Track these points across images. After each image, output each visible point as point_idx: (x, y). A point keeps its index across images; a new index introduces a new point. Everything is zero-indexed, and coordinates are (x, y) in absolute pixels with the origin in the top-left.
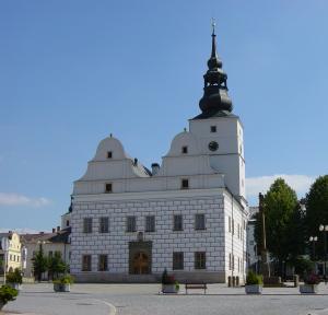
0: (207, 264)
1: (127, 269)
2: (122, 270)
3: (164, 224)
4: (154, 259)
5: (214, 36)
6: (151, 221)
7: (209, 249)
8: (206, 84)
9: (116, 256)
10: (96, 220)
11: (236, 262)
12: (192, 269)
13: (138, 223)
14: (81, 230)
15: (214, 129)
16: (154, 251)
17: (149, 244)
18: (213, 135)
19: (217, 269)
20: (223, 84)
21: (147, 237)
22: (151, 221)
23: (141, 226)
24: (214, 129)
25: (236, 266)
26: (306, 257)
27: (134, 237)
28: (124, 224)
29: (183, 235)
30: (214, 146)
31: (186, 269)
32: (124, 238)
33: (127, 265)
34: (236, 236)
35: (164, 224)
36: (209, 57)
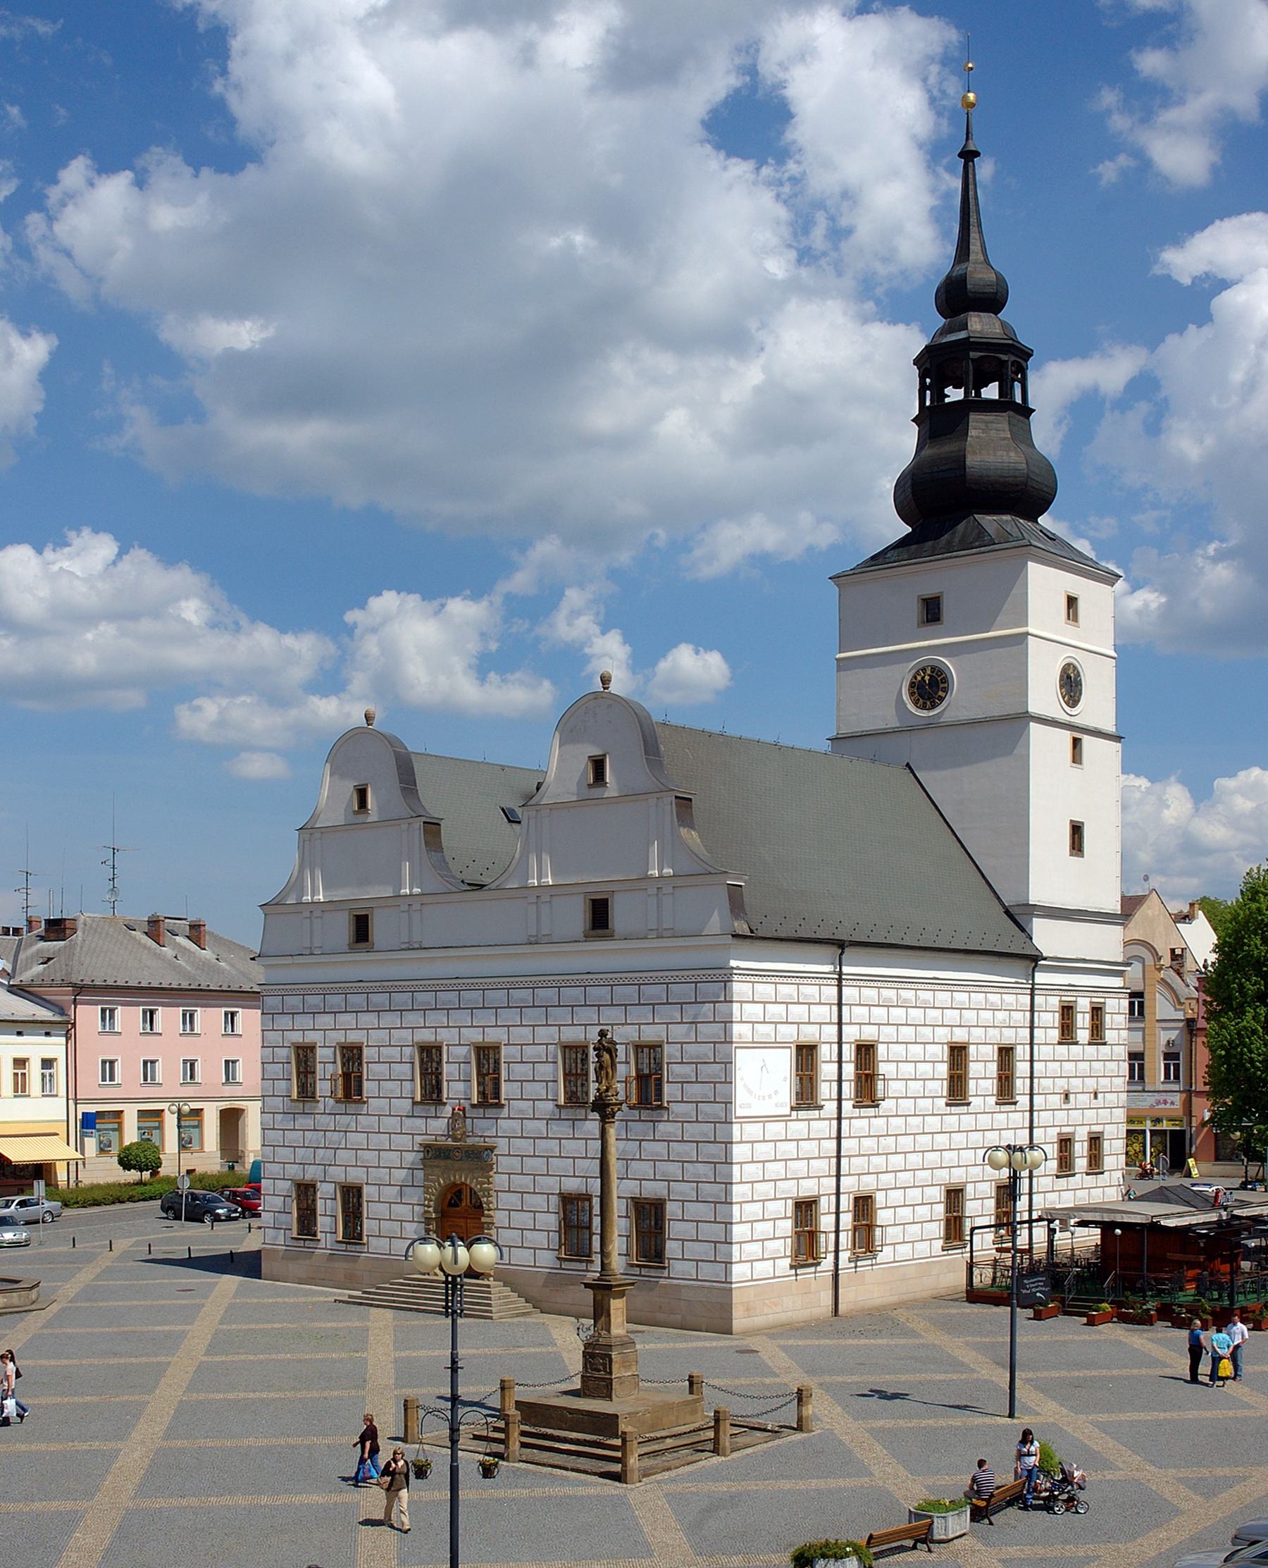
16: (499, 1181)
17: (480, 1157)
23: (459, 1085)
35: (533, 1080)
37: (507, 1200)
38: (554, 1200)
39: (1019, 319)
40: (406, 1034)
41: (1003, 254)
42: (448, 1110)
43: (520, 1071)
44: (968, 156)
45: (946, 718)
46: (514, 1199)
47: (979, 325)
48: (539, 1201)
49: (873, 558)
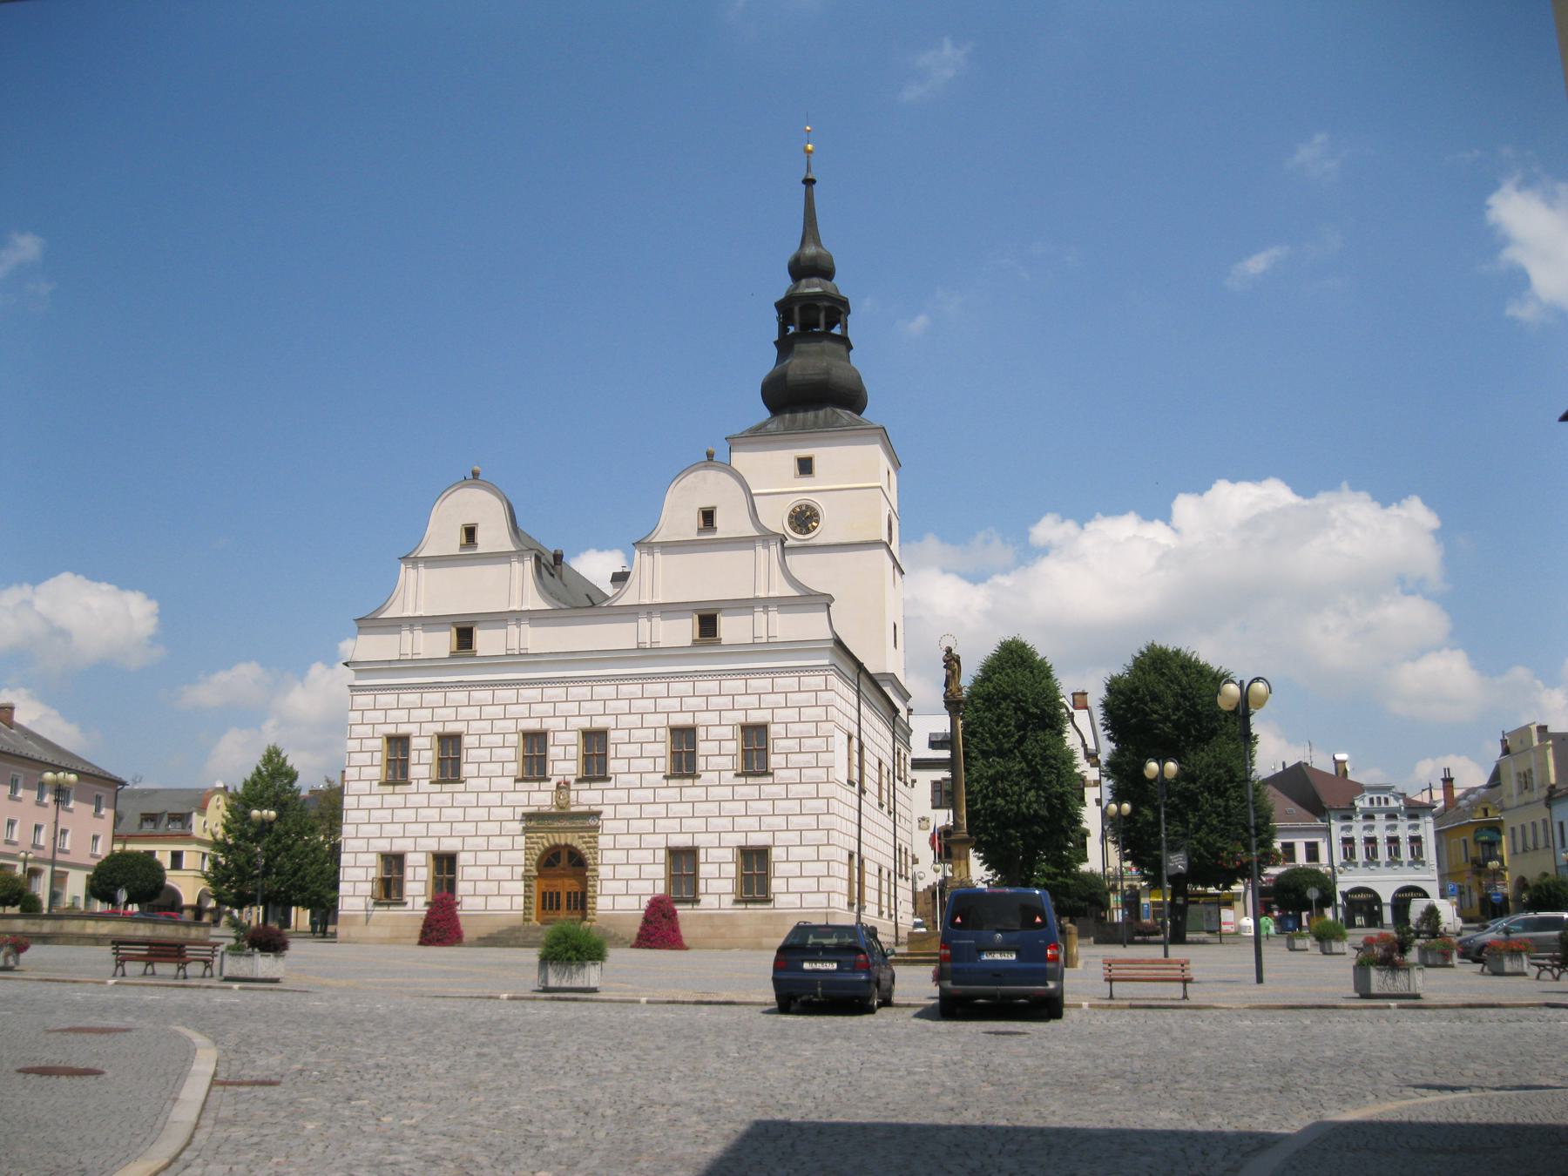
0: (776, 885)
1: (519, 902)
2: (504, 903)
3: (639, 755)
4: (604, 871)
5: (809, 182)
6: (595, 743)
7: (782, 837)
8: (783, 328)
9: (485, 857)
10: (426, 742)
11: (871, 881)
12: (728, 901)
13: (553, 752)
14: (377, 772)
15: (805, 466)
16: (604, 841)
17: (589, 819)
18: (806, 484)
19: (810, 900)
20: (837, 330)
21: (586, 797)
22: (595, 743)
23: (564, 760)
24: (805, 466)
25: (870, 895)
26: (1276, 913)
27: (542, 797)
28: (511, 756)
29: (698, 793)
30: (804, 519)
31: (707, 902)
32: (510, 797)
33: (519, 887)
34: (871, 798)
35: (639, 755)
36: (790, 247)
37: (609, 856)
38: (661, 854)
39: (842, 284)
40: (511, 725)
41: (832, 243)
42: (553, 783)
43: (625, 750)
44: (809, 182)
45: (819, 540)
46: (620, 856)
47: (813, 287)
48: (647, 855)
49: (750, 430)
